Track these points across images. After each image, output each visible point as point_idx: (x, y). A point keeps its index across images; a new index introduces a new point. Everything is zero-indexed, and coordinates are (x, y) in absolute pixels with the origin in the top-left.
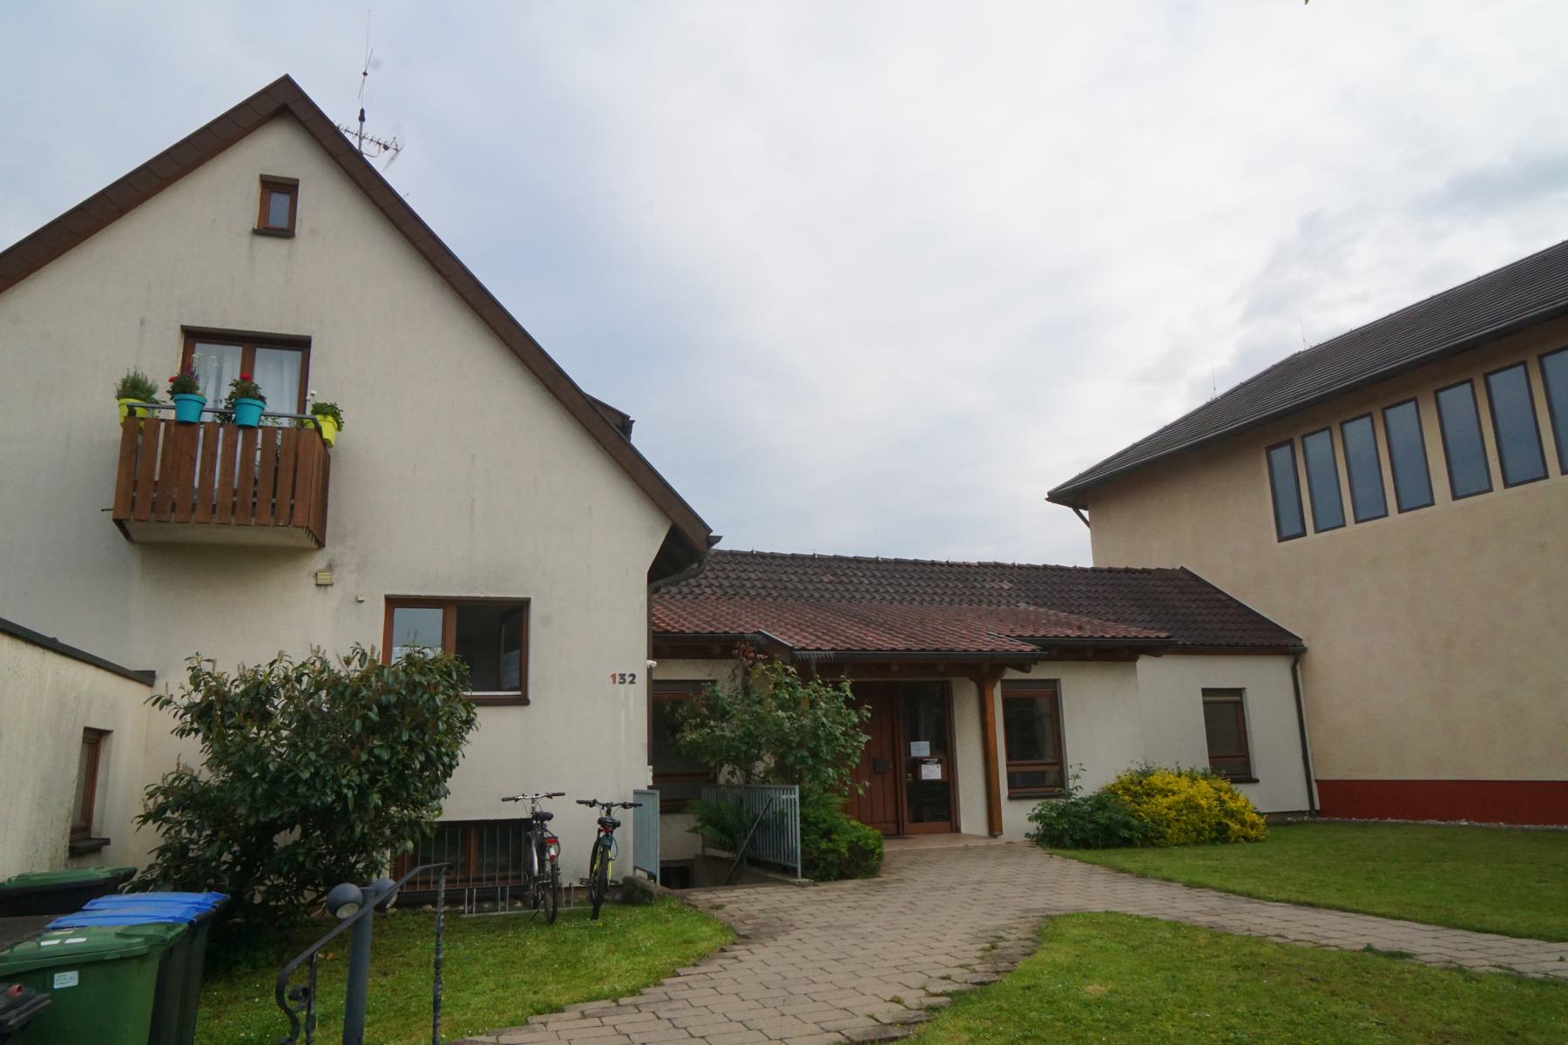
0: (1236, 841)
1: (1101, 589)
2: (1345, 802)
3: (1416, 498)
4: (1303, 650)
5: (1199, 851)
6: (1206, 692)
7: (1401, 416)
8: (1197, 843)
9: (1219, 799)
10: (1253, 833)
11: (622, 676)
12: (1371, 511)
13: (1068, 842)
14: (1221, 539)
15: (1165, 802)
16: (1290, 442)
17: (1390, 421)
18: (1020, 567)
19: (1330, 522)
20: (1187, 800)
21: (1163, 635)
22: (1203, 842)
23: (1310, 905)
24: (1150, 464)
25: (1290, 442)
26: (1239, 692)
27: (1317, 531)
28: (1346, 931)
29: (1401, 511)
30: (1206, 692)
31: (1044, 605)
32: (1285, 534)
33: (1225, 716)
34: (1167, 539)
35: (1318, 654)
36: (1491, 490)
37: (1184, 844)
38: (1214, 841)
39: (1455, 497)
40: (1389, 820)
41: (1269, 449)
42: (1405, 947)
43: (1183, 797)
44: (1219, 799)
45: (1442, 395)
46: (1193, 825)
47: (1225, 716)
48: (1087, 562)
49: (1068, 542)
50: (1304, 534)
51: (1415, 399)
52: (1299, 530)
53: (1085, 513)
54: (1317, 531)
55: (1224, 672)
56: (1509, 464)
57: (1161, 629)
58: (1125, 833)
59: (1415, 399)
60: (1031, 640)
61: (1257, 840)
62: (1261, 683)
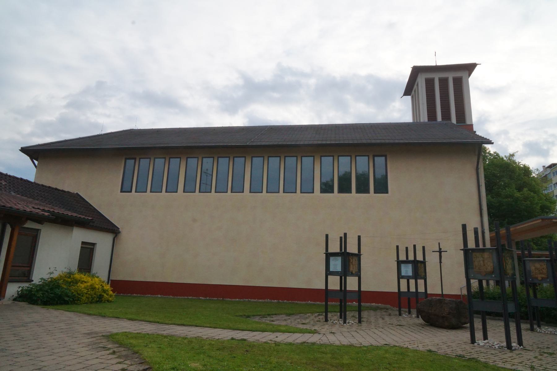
0: (104, 302)
1: (46, 194)
2: (123, 288)
3: (238, 189)
4: (119, 232)
5: (93, 306)
6: (83, 243)
7: (175, 162)
8: (91, 303)
9: (101, 285)
10: (111, 299)
11: (363, 188)
12: (156, 189)
13: (39, 302)
14: (98, 188)
15: (83, 286)
16: (135, 159)
17: (141, 162)
18: (10, 176)
19: (141, 190)
20: (91, 285)
21: (90, 218)
22: (93, 303)
23: (184, 325)
24: (64, 150)
25: (135, 159)
26: (94, 244)
27: (136, 192)
28: (225, 334)
29: (166, 192)
30: (83, 243)
31: (30, 197)
32: (123, 190)
33: (87, 252)
34: (71, 180)
35: (124, 234)
36: (262, 192)
37: (86, 303)
38: (97, 302)
39: (184, 192)
40: (135, 295)
41: (126, 159)
42: (245, 338)
43: (89, 284)
44: (101, 285)
45: (189, 159)
46: (91, 295)
47: (87, 252)
48: (33, 181)
49: (26, 169)
50: (131, 192)
51: (180, 158)
52: (130, 190)
53: (36, 162)
54: (136, 192)
55: (90, 236)
56: (125, 183)
57: (89, 216)
58: (67, 299)
59: (180, 158)
60: (48, 211)
61: (111, 301)
62: (102, 241)
